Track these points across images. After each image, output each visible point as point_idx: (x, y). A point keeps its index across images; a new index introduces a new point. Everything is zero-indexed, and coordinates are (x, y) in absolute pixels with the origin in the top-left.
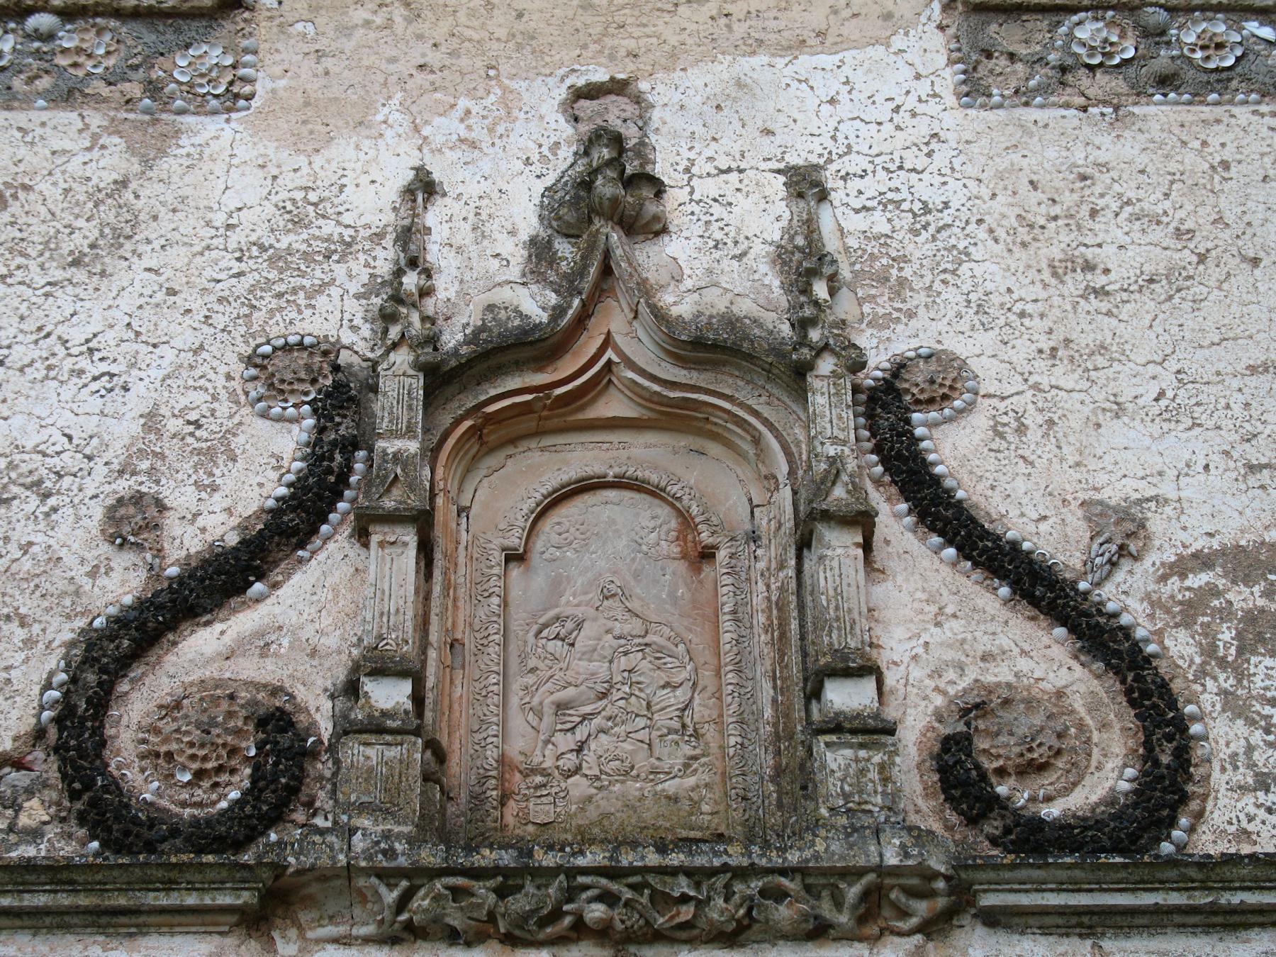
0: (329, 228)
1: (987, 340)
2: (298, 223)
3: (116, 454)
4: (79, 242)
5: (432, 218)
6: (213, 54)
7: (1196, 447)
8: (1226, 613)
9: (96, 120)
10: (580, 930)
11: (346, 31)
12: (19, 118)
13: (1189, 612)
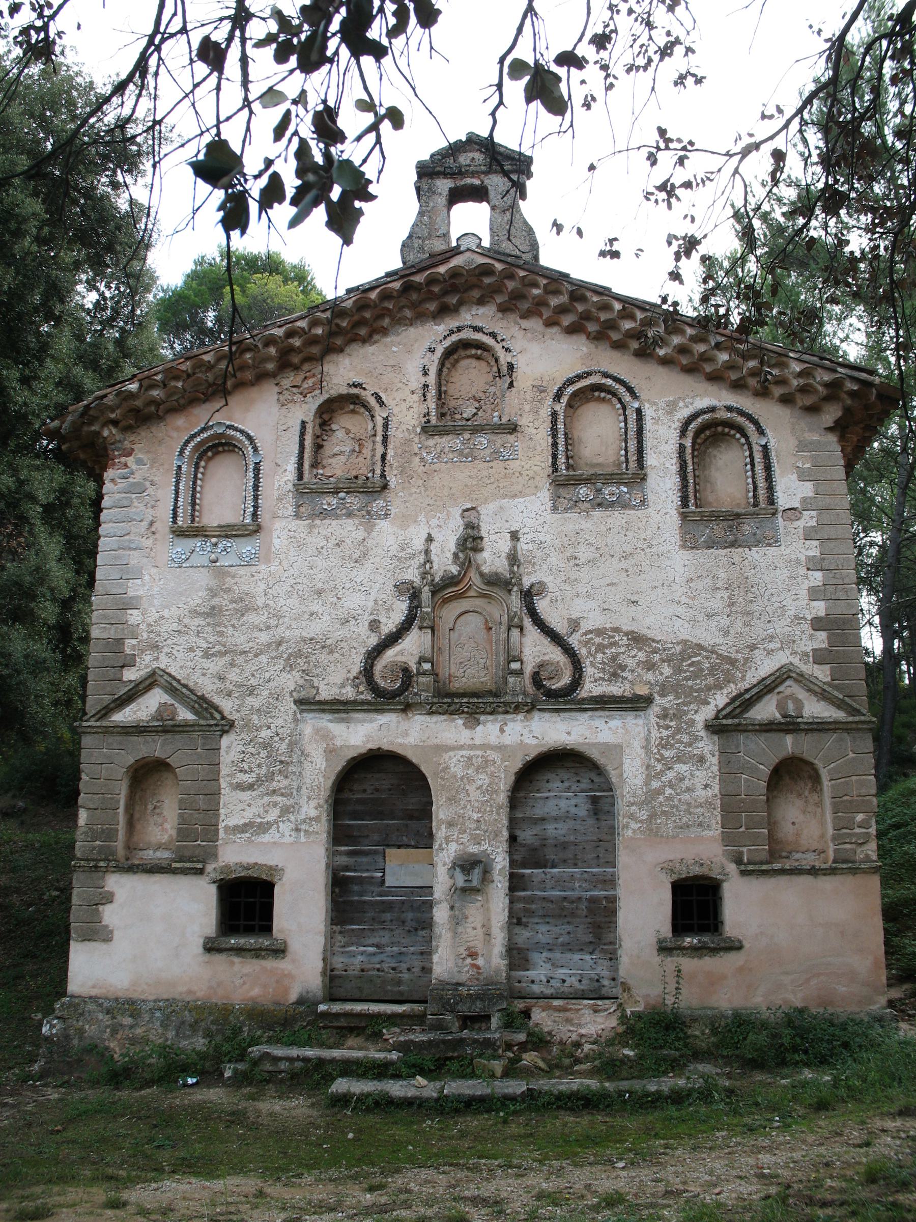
0: (410, 551)
1: (551, 578)
2: (403, 549)
3: (369, 610)
4: (356, 556)
5: (432, 547)
6: (381, 503)
7: (593, 604)
8: (593, 644)
9: (357, 522)
10: (463, 712)
11: (411, 494)
12: (340, 522)
13: (586, 643)
